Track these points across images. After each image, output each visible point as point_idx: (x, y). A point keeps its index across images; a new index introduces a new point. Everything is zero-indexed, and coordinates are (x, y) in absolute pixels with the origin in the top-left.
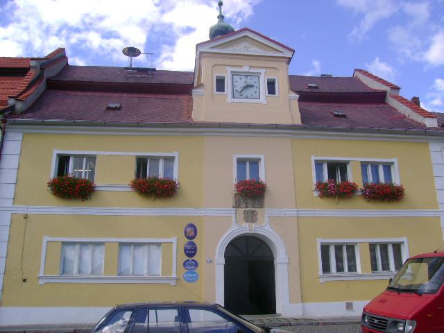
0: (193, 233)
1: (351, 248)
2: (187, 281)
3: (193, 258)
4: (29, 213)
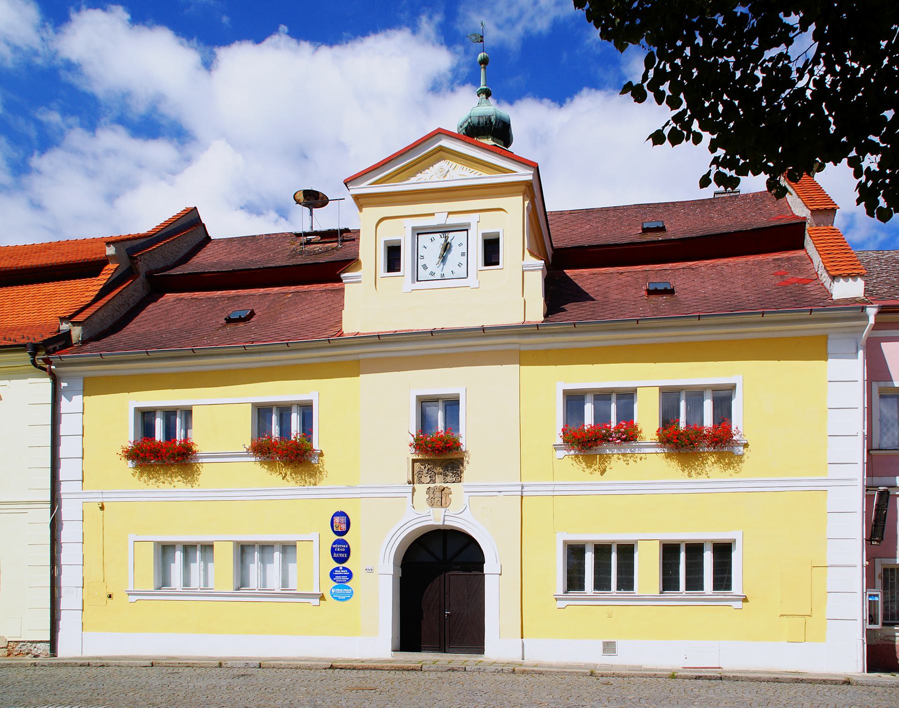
0: (344, 527)
1: (627, 551)
2: (337, 598)
3: (344, 565)
4: (105, 500)
